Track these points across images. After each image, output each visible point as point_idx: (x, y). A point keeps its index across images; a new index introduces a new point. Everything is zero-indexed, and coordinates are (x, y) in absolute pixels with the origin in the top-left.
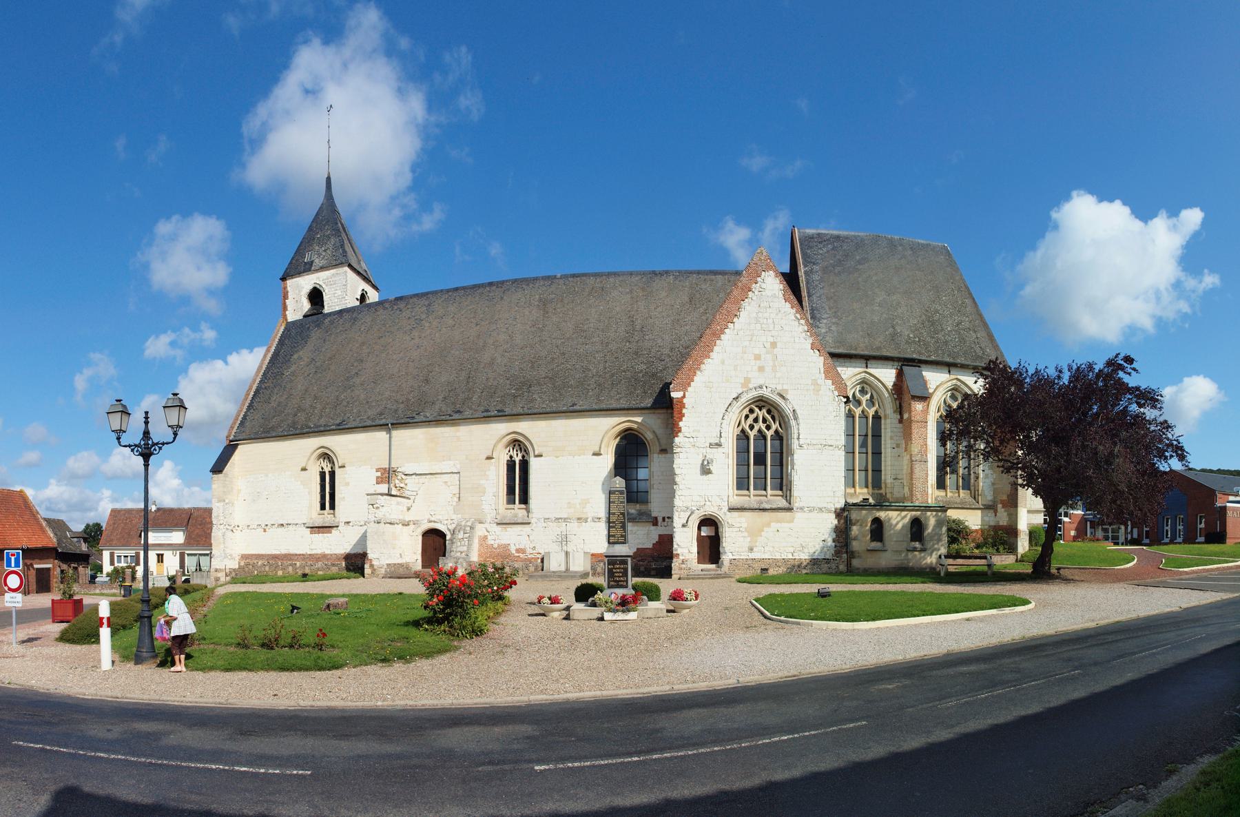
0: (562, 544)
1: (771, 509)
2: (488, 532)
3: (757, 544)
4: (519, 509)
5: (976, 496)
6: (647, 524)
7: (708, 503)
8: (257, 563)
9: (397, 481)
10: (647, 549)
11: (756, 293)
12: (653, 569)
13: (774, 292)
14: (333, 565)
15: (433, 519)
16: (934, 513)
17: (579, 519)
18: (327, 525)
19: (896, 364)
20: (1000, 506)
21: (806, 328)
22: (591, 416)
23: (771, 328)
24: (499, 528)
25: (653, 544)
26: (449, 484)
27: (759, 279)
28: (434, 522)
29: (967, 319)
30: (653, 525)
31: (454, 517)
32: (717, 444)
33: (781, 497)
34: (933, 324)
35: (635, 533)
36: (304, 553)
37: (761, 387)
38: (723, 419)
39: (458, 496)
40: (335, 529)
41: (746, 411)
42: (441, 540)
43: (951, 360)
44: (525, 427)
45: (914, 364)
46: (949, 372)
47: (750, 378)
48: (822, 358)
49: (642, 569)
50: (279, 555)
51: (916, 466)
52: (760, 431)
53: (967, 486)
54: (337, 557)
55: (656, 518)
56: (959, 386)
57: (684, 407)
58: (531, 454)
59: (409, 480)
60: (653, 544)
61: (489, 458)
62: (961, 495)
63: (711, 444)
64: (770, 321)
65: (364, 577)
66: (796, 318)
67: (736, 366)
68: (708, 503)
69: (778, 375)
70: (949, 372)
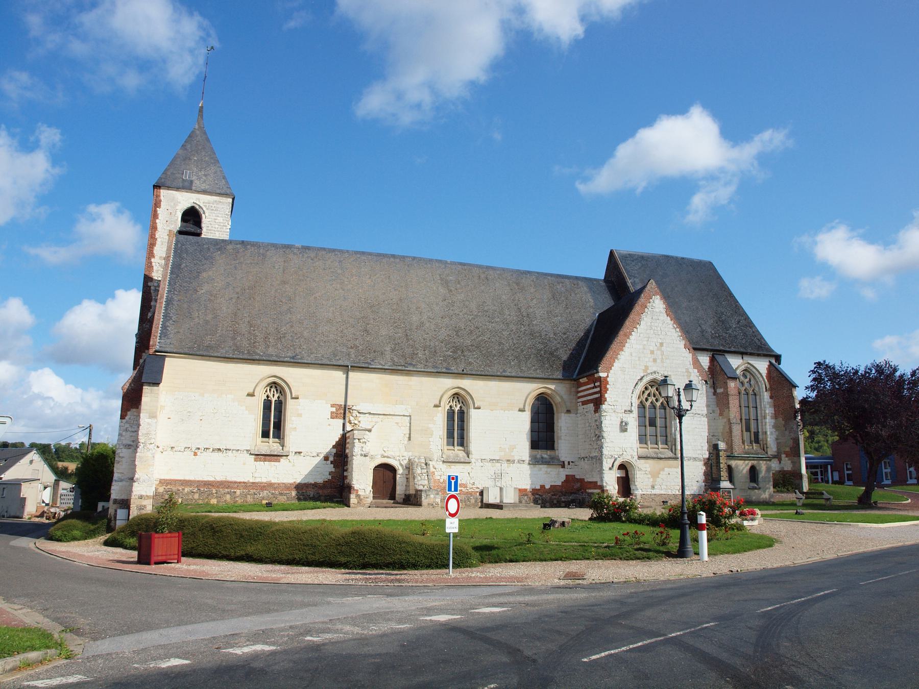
0: (495, 480)
1: (665, 458)
2: (435, 469)
3: (656, 483)
4: (458, 450)
5: (765, 448)
6: (557, 466)
7: (624, 453)
8: (183, 489)
9: (352, 418)
10: (558, 486)
11: (650, 309)
12: (563, 502)
13: (660, 309)
14: (281, 494)
15: (386, 454)
16: (765, 462)
17: (508, 461)
18: (275, 453)
19: (709, 353)
20: (783, 456)
21: (680, 334)
22: (523, 382)
23: (660, 334)
24: (445, 465)
25: (562, 482)
26: (400, 425)
27: (651, 300)
28: (388, 457)
29: (743, 318)
30: (562, 468)
31: (405, 454)
32: (629, 411)
33: (667, 450)
34: (723, 322)
35: (549, 474)
36: (246, 481)
37: (655, 372)
38: (632, 393)
39: (408, 436)
40: (285, 458)
41: (643, 389)
42: (391, 474)
43: (744, 351)
44: (467, 384)
45: (720, 353)
46: (742, 358)
47: (648, 366)
48: (691, 354)
49: (555, 502)
50: (213, 482)
51: (734, 427)
52: (652, 403)
53: (757, 441)
54: (287, 487)
55: (564, 462)
56: (749, 368)
57: (608, 384)
58: (472, 406)
59: (362, 418)
60: (562, 482)
61: (436, 406)
62: (755, 448)
63: (625, 411)
64: (659, 329)
65: (349, 507)
66: (674, 327)
67: (639, 358)
68: (624, 453)
69: (665, 365)
70: (742, 358)
